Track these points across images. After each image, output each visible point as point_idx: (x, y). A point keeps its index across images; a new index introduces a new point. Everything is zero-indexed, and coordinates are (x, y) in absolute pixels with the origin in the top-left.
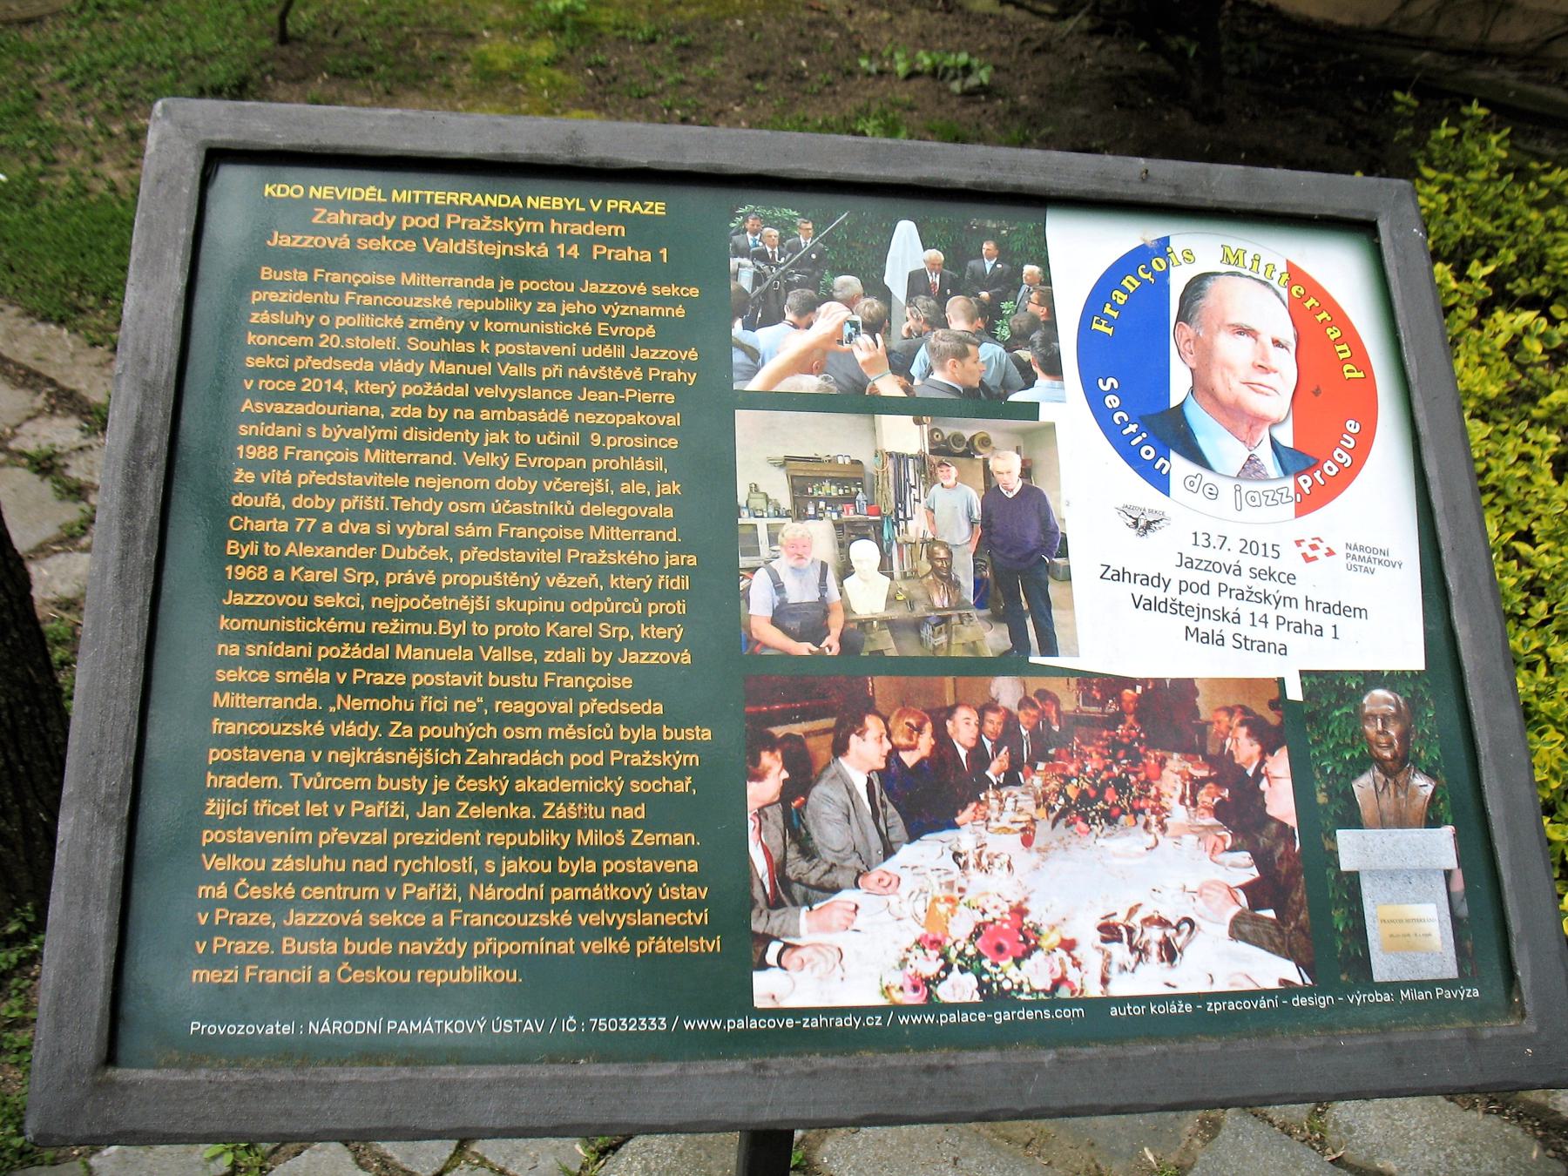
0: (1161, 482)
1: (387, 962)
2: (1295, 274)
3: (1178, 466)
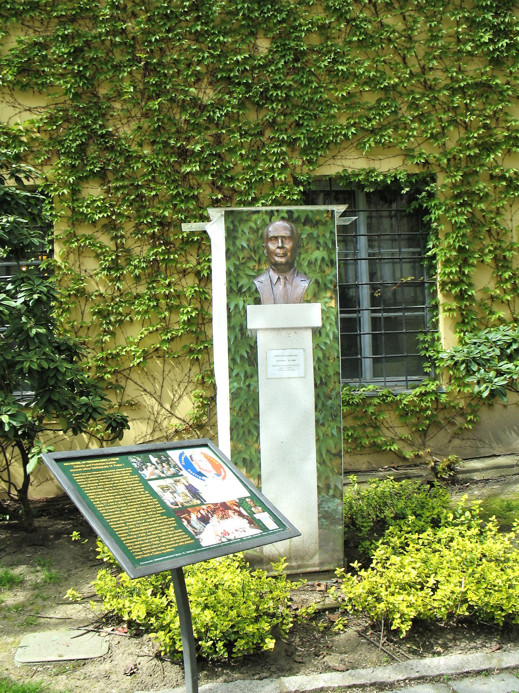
1: (158, 551)
2: (202, 453)
3: (203, 478)
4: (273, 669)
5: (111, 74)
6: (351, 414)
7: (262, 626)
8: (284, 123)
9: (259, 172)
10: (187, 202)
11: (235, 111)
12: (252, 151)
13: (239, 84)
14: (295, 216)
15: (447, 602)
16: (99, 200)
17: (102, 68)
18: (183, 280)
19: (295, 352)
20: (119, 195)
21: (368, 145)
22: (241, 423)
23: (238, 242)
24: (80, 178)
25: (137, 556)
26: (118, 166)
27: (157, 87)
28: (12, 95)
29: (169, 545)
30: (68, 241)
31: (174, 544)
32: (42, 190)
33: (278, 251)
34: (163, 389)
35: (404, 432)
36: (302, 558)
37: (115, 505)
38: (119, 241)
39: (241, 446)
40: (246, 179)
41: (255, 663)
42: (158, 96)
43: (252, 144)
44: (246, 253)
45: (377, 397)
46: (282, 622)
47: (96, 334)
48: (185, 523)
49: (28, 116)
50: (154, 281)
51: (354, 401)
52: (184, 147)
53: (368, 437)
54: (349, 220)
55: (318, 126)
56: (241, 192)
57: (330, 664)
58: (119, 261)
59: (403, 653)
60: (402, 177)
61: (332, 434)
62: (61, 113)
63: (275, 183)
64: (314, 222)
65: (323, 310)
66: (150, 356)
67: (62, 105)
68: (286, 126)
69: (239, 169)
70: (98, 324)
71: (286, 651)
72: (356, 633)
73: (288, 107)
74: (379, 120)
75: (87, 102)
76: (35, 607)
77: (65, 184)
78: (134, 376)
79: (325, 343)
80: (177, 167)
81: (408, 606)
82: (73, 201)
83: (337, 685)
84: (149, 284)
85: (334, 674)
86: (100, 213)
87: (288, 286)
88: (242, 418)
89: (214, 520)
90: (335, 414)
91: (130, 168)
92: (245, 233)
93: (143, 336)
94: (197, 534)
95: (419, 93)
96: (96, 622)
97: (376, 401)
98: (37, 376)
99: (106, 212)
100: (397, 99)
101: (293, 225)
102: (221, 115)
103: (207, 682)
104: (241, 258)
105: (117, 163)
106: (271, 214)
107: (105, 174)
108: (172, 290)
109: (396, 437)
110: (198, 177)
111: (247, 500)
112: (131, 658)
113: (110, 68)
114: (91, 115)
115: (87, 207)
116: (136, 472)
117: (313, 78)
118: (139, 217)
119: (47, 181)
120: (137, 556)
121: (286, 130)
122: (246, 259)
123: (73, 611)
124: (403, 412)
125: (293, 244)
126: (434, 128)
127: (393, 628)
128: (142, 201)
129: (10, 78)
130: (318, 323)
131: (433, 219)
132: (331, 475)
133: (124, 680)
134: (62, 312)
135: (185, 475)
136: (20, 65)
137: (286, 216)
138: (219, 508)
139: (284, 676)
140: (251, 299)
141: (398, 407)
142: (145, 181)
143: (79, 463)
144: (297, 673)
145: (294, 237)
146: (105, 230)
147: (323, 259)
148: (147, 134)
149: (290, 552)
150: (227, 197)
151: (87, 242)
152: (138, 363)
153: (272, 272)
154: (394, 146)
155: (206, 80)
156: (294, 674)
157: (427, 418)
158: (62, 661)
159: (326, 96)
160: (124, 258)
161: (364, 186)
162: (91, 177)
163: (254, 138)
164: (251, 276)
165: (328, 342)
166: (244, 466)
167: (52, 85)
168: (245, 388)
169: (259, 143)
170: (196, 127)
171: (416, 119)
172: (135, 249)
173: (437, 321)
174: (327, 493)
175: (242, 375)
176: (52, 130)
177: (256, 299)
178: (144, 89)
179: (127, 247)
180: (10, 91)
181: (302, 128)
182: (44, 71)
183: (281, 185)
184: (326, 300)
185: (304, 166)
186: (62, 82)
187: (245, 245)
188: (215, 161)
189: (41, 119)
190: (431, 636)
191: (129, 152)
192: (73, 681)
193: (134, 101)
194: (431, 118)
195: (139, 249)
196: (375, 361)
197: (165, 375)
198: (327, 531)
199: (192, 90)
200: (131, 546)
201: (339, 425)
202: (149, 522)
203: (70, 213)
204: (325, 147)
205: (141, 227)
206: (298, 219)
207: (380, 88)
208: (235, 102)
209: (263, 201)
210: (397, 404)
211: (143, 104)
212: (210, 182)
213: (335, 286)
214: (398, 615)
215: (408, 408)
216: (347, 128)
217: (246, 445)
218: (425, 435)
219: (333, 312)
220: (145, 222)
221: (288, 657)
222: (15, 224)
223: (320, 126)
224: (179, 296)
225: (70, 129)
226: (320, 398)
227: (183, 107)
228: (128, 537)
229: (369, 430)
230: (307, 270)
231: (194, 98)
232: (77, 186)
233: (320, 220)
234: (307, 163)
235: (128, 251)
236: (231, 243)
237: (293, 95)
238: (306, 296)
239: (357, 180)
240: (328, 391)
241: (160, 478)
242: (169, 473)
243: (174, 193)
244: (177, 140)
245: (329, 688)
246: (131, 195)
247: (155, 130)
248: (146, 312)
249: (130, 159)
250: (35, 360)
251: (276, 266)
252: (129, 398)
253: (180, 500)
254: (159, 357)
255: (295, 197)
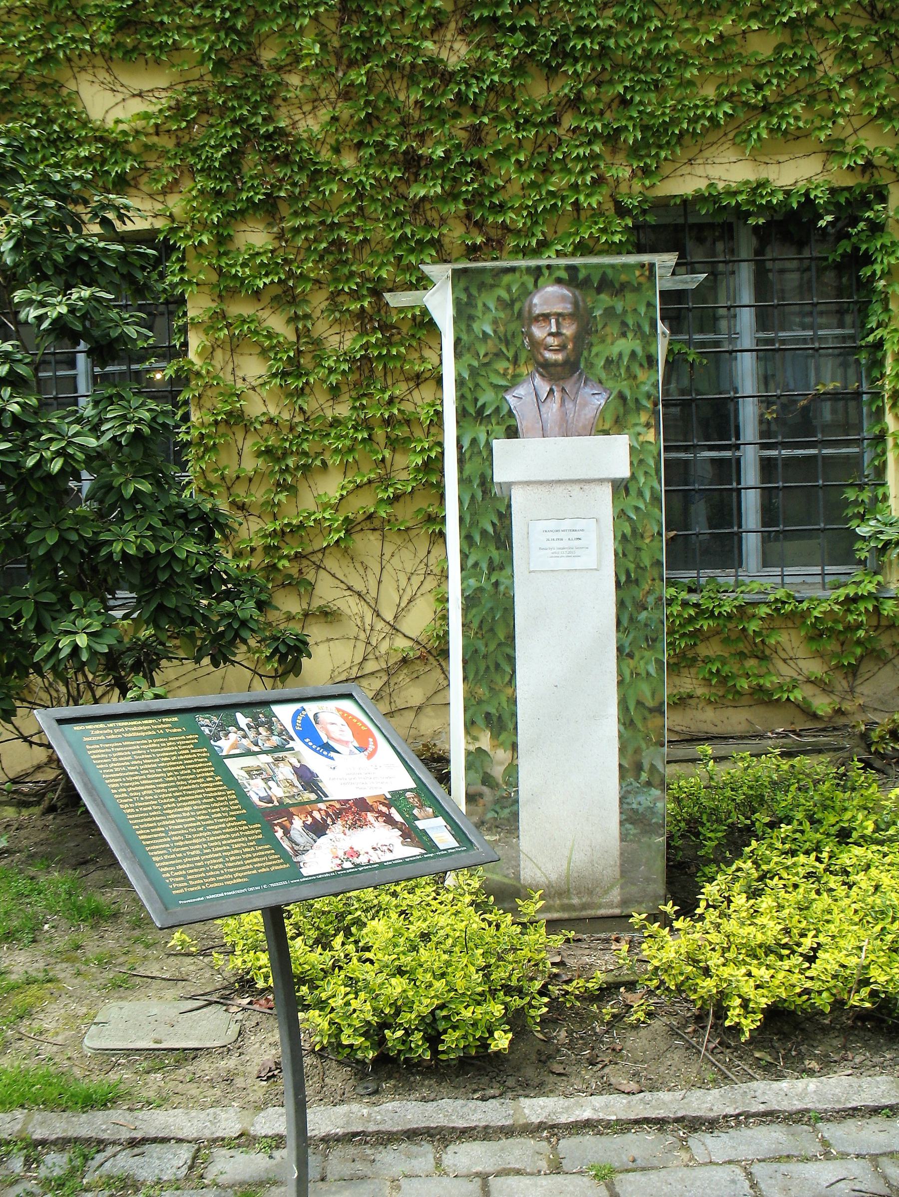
0: (332, 758)
1: (217, 882)
2: (339, 710)
3: (332, 754)
4: (511, 1082)
5: (280, 22)
6: (718, 633)
7: (490, 1009)
8: (598, 100)
9: (550, 193)
10: (421, 252)
11: (506, 80)
12: (539, 154)
13: (513, 29)
14: (582, 275)
15: (833, 983)
16: (265, 252)
17: (265, 12)
18: (416, 393)
19: (581, 524)
20: (300, 241)
21: (755, 136)
22: (483, 650)
23: (476, 326)
24: (230, 214)
25: (177, 888)
26: (297, 191)
27: (363, 42)
28: (109, 70)
29: (240, 872)
30: (212, 327)
31: (250, 870)
32: (165, 237)
33: (550, 340)
34: (382, 586)
35: (814, 668)
36: (590, 892)
37: (154, 800)
38: (300, 326)
39: (482, 691)
40: (528, 207)
41: (481, 1071)
42: (366, 59)
43: (539, 142)
44: (491, 346)
45: (765, 603)
46: (529, 1003)
47: (263, 490)
48: (279, 833)
49: (137, 106)
50: (364, 395)
51: (722, 610)
52: (414, 151)
53: (747, 676)
54: (692, 281)
55: (661, 103)
56: (520, 231)
57: (613, 1080)
58: (302, 361)
59: (746, 1068)
60: (820, 196)
61: (648, 674)
62: (195, 99)
63: (582, 212)
64: (617, 286)
65: (632, 448)
66: (359, 528)
67: (196, 84)
68: (601, 106)
69: (514, 189)
70: (267, 472)
71: (539, 1052)
72: (668, 1028)
73: (604, 69)
74: (778, 86)
75: (241, 76)
76: (130, 958)
77: (205, 225)
78: (330, 563)
79: (637, 509)
80: (402, 189)
81: (757, 987)
82: (220, 255)
83: (614, 1118)
84: (355, 400)
85: (623, 1100)
86: (267, 275)
87: (569, 405)
88: (483, 642)
89: (336, 831)
90: (654, 636)
91: (319, 192)
92: (488, 308)
93: (344, 493)
94: (297, 853)
95: (857, 29)
96: (225, 988)
97: (763, 611)
98: (138, 567)
99: (277, 273)
100: (814, 44)
101: (577, 293)
102: (481, 90)
103: (393, 1100)
104: (482, 354)
105: (294, 184)
106: (537, 272)
107: (275, 206)
108: (396, 412)
109: (800, 677)
110: (439, 205)
111: (408, 794)
112: (274, 1052)
113: (279, 10)
114: (248, 99)
115: (244, 265)
116: (204, 741)
117: (653, 11)
118: (337, 280)
119: (173, 221)
120: (177, 888)
121: (602, 113)
122: (490, 356)
123: (192, 968)
124: (811, 632)
125: (578, 327)
126: (885, 97)
127: (727, 1023)
128: (340, 252)
129: (105, 38)
130: (623, 471)
131: (879, 273)
132: (644, 746)
133: (255, 1088)
134: (204, 453)
135: (296, 749)
136: (120, 13)
137: (564, 275)
138: (351, 808)
139: (527, 1096)
140: (501, 429)
141: (804, 623)
142: (346, 215)
143: (102, 725)
144: (551, 1091)
145: (580, 315)
146: (275, 304)
147: (633, 354)
148: (348, 129)
149: (568, 880)
150: (493, 241)
151: (246, 327)
152: (337, 541)
153: (538, 380)
154: (806, 136)
155: (453, 25)
156: (544, 1094)
157: (859, 642)
158: (158, 1050)
159: (677, 45)
160: (311, 355)
161: (748, 214)
162: (251, 211)
163: (541, 131)
164: (501, 386)
165: (642, 506)
166: (487, 726)
167: (176, 47)
168: (489, 587)
169: (552, 139)
170: (435, 113)
171: (853, 80)
172: (330, 339)
173: (885, 463)
174: (637, 777)
175: (484, 566)
176: (179, 129)
177: (509, 428)
178: (342, 47)
179: (315, 335)
180: (106, 61)
181: (632, 108)
182: (162, 23)
183: (592, 216)
184: (639, 429)
185: (635, 180)
186: (194, 41)
187: (489, 330)
188: (471, 175)
189: (161, 111)
190: (802, 1042)
191: (316, 163)
192: (171, 1085)
193: (323, 70)
194: (881, 76)
195: (337, 338)
196: (767, 539)
197: (384, 563)
198: (635, 846)
199: (428, 45)
200: (169, 872)
201: (660, 657)
202: (210, 830)
203: (214, 277)
204: (673, 142)
205: (340, 299)
206: (587, 281)
207: (781, 22)
208: (506, 64)
209: (559, 247)
210: (802, 617)
211: (340, 74)
212: (462, 214)
213: (656, 404)
214: (738, 1001)
215: (822, 624)
216: (717, 104)
217: (491, 689)
218: (855, 675)
219: (651, 451)
220: (346, 290)
221: (540, 1064)
222: (94, 303)
223: (665, 101)
224: (408, 422)
225: (212, 126)
226: (627, 608)
227: (411, 76)
228: (166, 857)
229: (751, 663)
230: (603, 376)
231: (432, 60)
232: (225, 228)
233: (628, 282)
234: (640, 173)
235: (318, 343)
236: (463, 327)
237: (613, 46)
238: (601, 422)
239: (734, 203)
240: (640, 594)
241: (248, 753)
242: (268, 745)
243: (398, 235)
244: (403, 139)
245: (599, 1121)
246: (321, 242)
247: (361, 122)
248: (351, 450)
249: (318, 177)
250: (132, 539)
251: (547, 369)
252: (322, 603)
253: (278, 792)
254: (374, 530)
255: (617, 238)
